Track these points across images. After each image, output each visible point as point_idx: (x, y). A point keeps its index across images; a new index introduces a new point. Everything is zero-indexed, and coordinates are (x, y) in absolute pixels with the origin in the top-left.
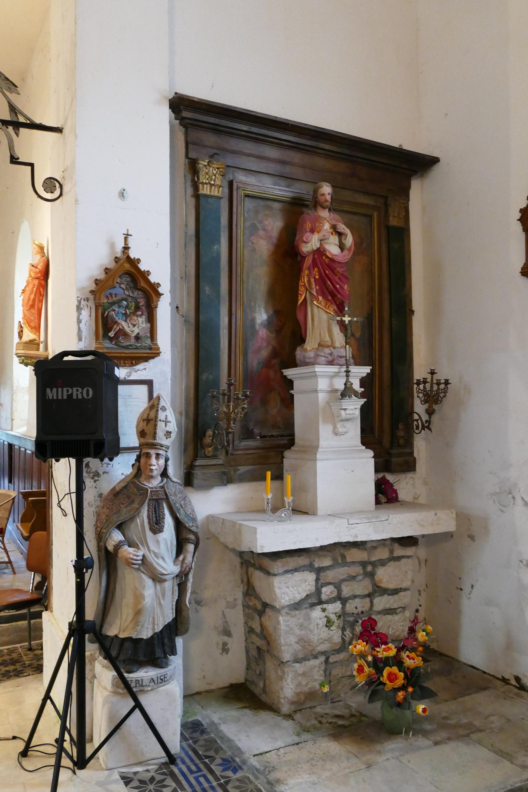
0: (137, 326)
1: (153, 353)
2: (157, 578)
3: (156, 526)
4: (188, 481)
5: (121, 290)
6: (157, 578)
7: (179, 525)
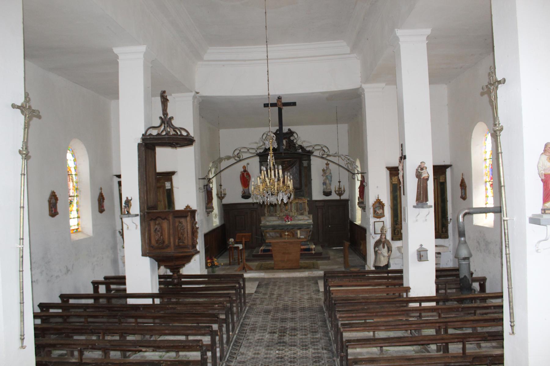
0: (380, 212)
1: (383, 216)
2: (384, 256)
3: (384, 247)
4: (393, 239)
5: (377, 205)
6: (384, 256)
7: (388, 248)
